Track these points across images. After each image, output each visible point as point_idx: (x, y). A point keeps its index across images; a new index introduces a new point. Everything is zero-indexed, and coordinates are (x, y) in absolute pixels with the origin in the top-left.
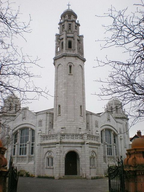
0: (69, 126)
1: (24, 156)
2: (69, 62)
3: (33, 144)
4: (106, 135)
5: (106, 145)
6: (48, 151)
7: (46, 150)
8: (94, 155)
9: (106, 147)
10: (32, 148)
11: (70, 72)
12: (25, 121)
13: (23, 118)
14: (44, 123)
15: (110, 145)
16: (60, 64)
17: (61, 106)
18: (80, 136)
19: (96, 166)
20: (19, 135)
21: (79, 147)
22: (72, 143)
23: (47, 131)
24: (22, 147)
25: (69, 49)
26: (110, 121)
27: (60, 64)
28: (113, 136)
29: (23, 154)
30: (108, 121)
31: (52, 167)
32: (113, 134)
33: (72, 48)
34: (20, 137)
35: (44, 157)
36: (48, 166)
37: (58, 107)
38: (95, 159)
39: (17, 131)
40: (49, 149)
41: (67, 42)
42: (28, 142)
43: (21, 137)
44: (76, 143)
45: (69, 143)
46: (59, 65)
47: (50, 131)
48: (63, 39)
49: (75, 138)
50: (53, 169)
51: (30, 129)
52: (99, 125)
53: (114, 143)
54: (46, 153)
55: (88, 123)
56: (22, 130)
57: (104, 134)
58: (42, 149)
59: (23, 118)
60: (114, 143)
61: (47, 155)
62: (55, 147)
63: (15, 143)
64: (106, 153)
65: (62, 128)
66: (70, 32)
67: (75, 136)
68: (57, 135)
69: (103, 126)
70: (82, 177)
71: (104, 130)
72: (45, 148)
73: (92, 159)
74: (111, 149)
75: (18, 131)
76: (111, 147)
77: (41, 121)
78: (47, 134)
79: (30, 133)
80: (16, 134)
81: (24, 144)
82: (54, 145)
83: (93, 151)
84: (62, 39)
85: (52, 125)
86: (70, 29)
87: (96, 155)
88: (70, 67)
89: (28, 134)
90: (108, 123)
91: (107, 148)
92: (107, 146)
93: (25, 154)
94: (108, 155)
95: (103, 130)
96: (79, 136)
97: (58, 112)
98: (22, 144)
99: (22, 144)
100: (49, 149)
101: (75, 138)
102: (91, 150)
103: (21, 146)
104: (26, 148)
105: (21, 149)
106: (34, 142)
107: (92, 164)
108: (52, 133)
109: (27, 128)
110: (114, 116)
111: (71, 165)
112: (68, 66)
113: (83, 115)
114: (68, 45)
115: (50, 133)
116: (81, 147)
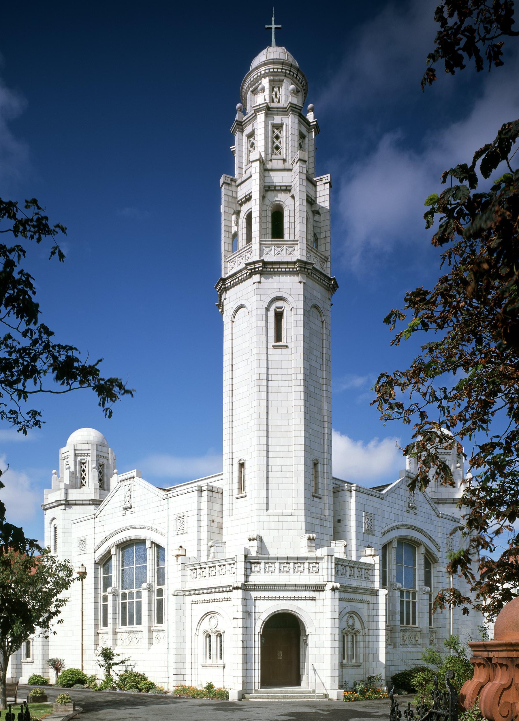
0: (276, 533)
1: (135, 627)
2: (273, 296)
3: (160, 592)
4: (399, 560)
5: (398, 593)
6: (206, 614)
7: (201, 609)
8: (358, 626)
9: (398, 600)
10: (160, 603)
11: (278, 338)
12: (130, 519)
13: (126, 509)
14: (191, 522)
15: (412, 590)
16: (241, 307)
17: (246, 465)
18: (309, 563)
19: (361, 660)
20: (115, 562)
21: (305, 599)
22: (285, 587)
23: (204, 548)
24: (403, 565)
25: (276, 241)
26: (415, 514)
27: (241, 307)
28: (423, 562)
29: (131, 623)
30: (408, 512)
31: (220, 662)
32: (422, 558)
33: (286, 237)
34: (121, 568)
35: (194, 631)
36: (210, 658)
37: (236, 467)
38: (360, 638)
39: (109, 552)
40: (211, 607)
41: (264, 226)
42: (144, 585)
43: (123, 570)
44: (296, 588)
45: (274, 588)
46: (236, 311)
47: (212, 549)
48: (250, 198)
49: (208, 575)
50: (224, 667)
51: (148, 544)
52: (376, 528)
53: (426, 585)
54: (202, 619)
55: (339, 521)
56: (125, 546)
57: (392, 555)
58: (188, 607)
59: (126, 509)
60: (426, 585)
61: (206, 625)
62: (230, 599)
63: (105, 590)
64: (398, 617)
65: (250, 540)
66: (277, 164)
67: (292, 565)
68: (233, 562)
69: (398, 527)
70: (314, 692)
71: (395, 544)
72: (197, 602)
73: (350, 637)
74: (414, 604)
75: (113, 551)
76: (414, 597)
77: (181, 518)
78: (204, 559)
79: (150, 554)
80: (105, 561)
81: (134, 590)
82: (225, 595)
83: (352, 612)
84: (248, 198)
85: (216, 528)
86: (277, 148)
87: (362, 623)
88: (315, 465)
89: (145, 560)
90: (410, 520)
91: (402, 602)
92: (402, 595)
93: (139, 623)
94: (402, 622)
95: (390, 542)
96: (306, 565)
97: (236, 486)
98: (127, 591)
99: (127, 591)
100: (211, 607)
101: (292, 571)
102: (348, 610)
103: (124, 596)
104: (139, 604)
105: (124, 606)
106: (164, 584)
107: (350, 652)
108: (220, 556)
109: (142, 542)
110: (431, 495)
111: (280, 654)
112: (272, 314)
113: (320, 492)
114: (270, 225)
115: (212, 555)
116: (313, 599)
